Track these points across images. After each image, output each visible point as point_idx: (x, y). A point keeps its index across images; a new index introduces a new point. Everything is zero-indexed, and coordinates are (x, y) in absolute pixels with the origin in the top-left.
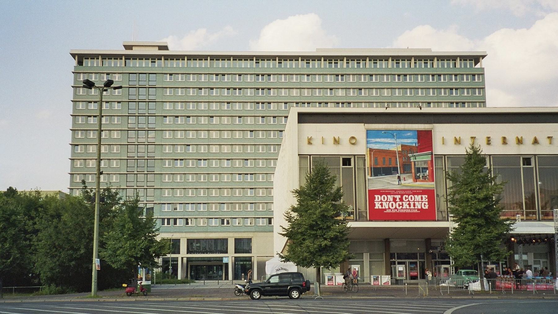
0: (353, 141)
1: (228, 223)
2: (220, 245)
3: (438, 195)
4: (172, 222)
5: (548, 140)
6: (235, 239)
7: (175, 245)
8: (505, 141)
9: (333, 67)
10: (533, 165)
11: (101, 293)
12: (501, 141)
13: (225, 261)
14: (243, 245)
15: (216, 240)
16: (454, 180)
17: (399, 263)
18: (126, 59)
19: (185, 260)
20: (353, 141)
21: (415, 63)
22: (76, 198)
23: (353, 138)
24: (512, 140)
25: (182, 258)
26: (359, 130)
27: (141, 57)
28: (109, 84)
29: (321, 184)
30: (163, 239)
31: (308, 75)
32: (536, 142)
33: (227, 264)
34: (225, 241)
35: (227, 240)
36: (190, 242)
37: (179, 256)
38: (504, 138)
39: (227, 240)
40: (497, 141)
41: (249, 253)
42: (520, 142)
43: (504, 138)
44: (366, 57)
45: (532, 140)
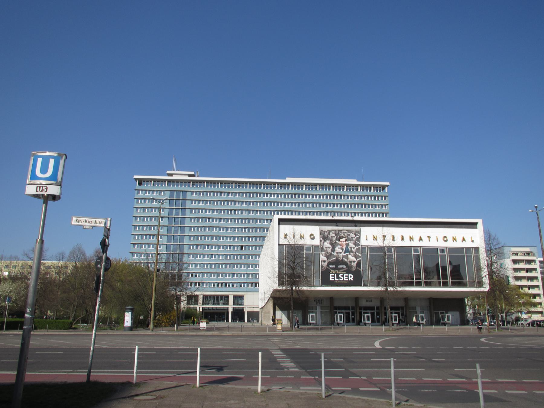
5: (428, 239)
8: (403, 239)
10: (445, 253)
11: (156, 329)
12: (400, 239)
14: (238, 299)
17: (339, 313)
19: (201, 309)
20: (312, 237)
23: (312, 235)
24: (407, 238)
26: (315, 230)
29: (293, 263)
32: (421, 239)
34: (227, 297)
36: (205, 297)
37: (198, 307)
38: (402, 236)
41: (241, 305)
42: (411, 239)
45: (418, 238)
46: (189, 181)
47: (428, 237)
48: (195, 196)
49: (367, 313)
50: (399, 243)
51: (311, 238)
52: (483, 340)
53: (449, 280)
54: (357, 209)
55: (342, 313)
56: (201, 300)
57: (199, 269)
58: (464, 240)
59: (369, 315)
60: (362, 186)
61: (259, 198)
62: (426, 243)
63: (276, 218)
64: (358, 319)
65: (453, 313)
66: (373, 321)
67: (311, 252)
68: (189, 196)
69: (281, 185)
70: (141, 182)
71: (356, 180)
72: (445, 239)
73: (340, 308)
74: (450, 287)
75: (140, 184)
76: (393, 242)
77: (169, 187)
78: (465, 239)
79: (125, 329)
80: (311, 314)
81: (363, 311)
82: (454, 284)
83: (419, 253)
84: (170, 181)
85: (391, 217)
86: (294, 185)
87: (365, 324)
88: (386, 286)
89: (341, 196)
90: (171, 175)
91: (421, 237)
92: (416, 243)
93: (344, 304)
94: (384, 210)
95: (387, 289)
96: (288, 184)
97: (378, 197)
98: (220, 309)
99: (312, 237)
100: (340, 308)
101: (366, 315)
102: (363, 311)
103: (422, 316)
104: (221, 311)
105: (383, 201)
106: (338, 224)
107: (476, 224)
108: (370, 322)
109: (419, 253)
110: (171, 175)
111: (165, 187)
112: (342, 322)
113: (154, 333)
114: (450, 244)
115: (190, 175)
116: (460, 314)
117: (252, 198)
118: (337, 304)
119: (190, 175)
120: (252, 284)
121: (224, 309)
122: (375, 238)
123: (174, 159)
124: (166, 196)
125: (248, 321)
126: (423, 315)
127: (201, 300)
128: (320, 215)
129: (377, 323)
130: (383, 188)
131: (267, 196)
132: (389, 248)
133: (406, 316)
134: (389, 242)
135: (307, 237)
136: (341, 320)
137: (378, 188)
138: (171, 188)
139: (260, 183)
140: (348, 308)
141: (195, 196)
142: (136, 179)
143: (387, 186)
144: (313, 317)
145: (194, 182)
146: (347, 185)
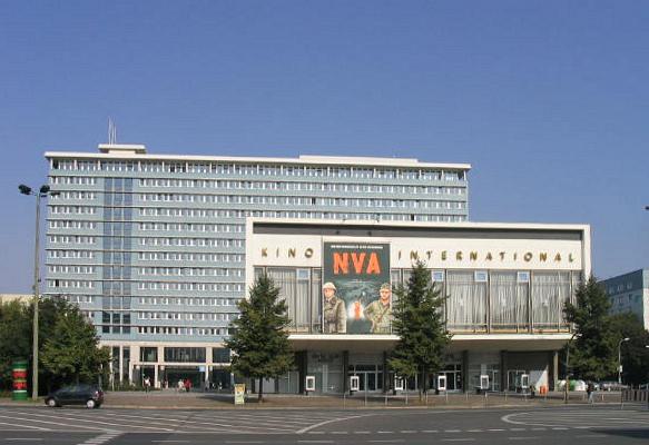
0: (309, 253)
1: (218, 332)
2: (198, 355)
4: (149, 330)
13: (202, 370)
15: (194, 349)
16: (399, 294)
23: (530, 254)
26: (315, 242)
27: (117, 161)
28: (45, 189)
30: (104, 347)
31: (278, 183)
33: (204, 373)
34: (202, 351)
35: (205, 349)
37: (156, 365)
39: (205, 349)
40: (436, 256)
43: (570, 256)
44: (350, 166)
46: (136, 161)
47: (460, 258)
49: (442, 374)
52: (505, 419)
56: (209, 356)
57: (154, 306)
59: (444, 377)
63: (250, 220)
68: (137, 186)
69: (290, 167)
70: (57, 162)
71: (416, 161)
75: (56, 166)
76: (569, 264)
79: (157, 389)
84: (104, 161)
90: (106, 151)
96: (301, 166)
101: (440, 377)
106: (373, 232)
107: (580, 232)
108: (313, 389)
110: (106, 151)
112: (313, 389)
115: (137, 151)
119: (137, 151)
120: (165, 328)
127: (209, 356)
130: (460, 173)
135: (496, 256)
142: (49, 158)
143: (467, 170)
145: (143, 162)
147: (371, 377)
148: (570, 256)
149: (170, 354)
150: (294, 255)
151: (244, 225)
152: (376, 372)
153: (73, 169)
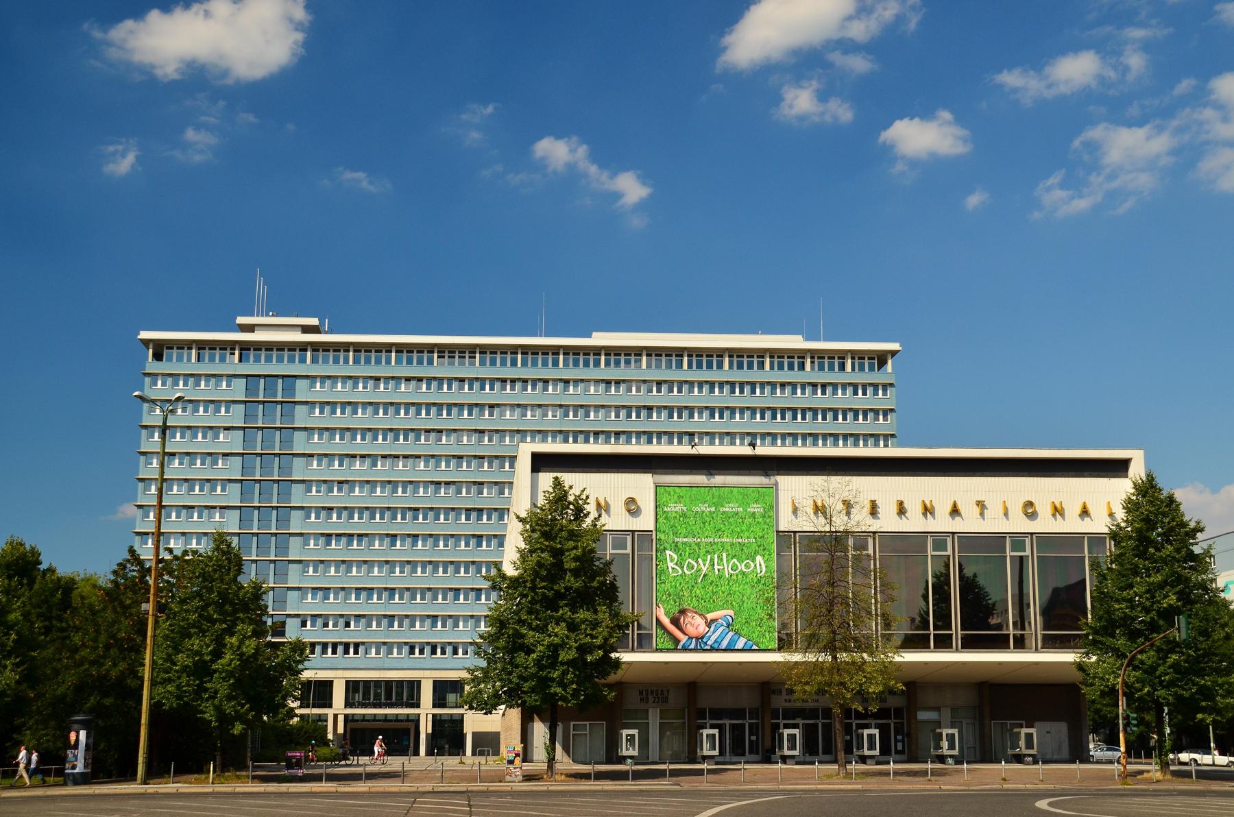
2: (407, 692)
3: (1214, 765)
5: (977, 510)
6: (434, 682)
7: (322, 693)
8: (902, 511)
9: (644, 366)
17: (787, 726)
18: (241, 349)
19: (341, 719)
20: (632, 507)
21: (812, 362)
22: (802, 118)
24: (914, 509)
25: (336, 716)
26: (641, 485)
27: (269, 346)
32: (955, 512)
34: (414, 685)
36: (352, 686)
38: (901, 503)
42: (928, 510)
43: (901, 503)
46: (303, 347)
48: (320, 392)
49: (867, 727)
50: (889, 522)
51: (629, 511)
52: (1042, 804)
53: (956, 630)
54: (699, 423)
55: (795, 726)
58: (1085, 513)
59: (876, 732)
60: (817, 355)
61: (509, 394)
62: (970, 523)
64: (768, 743)
65: (1047, 725)
66: (885, 751)
67: (629, 551)
68: (302, 391)
70: (160, 350)
72: (1030, 510)
73: (717, 713)
74: (1037, 651)
75: (158, 356)
77: (243, 365)
78: (1090, 509)
80: (625, 732)
81: (855, 722)
82: (970, 644)
83: (1028, 552)
84: (245, 347)
85: (901, 445)
86: (610, 351)
87: (784, 759)
88: (831, 648)
89: (865, 387)
90: (250, 328)
91: (955, 505)
92: (942, 523)
93: (728, 702)
94: (882, 425)
95: (835, 658)
96: (597, 351)
97: (865, 387)
98: (397, 718)
99: (632, 507)
100: (717, 713)
101: (866, 732)
102: (855, 722)
103: (949, 737)
104: (398, 725)
105: (882, 400)
108: (876, 752)
109: (949, 552)
110: (250, 328)
111: (233, 364)
112: (796, 753)
113: (152, 788)
114: (1046, 524)
115: (306, 329)
116: (1069, 729)
117: (488, 395)
118: (705, 702)
119: (306, 329)
121: (408, 718)
122: (819, 510)
123: (259, 280)
124: (238, 390)
125: (474, 754)
126: (955, 731)
128: (650, 442)
129: (748, 757)
130: (881, 359)
131: (824, 393)
132: (862, 539)
133: (909, 735)
134: (861, 521)
135: (618, 508)
136: (793, 747)
137: (866, 362)
138: (250, 368)
139: (556, 350)
140: (738, 713)
141: (320, 392)
142: (146, 342)
144: (631, 739)
145: (316, 347)
146: (773, 353)
147: (737, 731)
148: (982, 514)
149: (357, 691)
150: (1062, 515)
151: (513, 459)
152: (820, 723)
153: (190, 363)
